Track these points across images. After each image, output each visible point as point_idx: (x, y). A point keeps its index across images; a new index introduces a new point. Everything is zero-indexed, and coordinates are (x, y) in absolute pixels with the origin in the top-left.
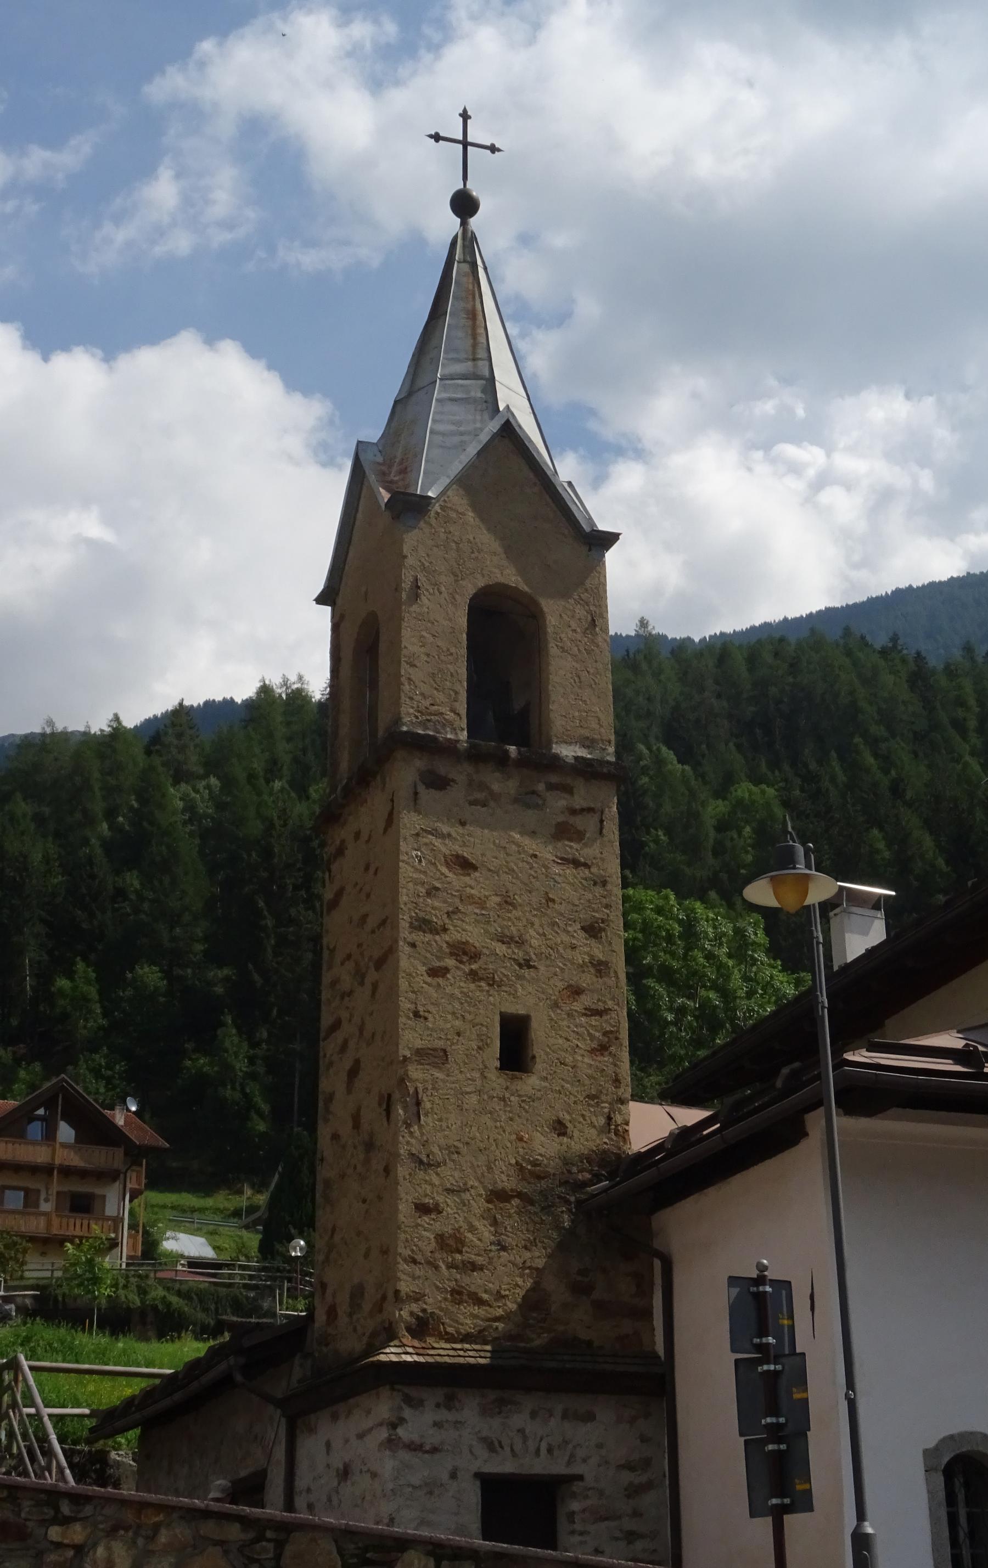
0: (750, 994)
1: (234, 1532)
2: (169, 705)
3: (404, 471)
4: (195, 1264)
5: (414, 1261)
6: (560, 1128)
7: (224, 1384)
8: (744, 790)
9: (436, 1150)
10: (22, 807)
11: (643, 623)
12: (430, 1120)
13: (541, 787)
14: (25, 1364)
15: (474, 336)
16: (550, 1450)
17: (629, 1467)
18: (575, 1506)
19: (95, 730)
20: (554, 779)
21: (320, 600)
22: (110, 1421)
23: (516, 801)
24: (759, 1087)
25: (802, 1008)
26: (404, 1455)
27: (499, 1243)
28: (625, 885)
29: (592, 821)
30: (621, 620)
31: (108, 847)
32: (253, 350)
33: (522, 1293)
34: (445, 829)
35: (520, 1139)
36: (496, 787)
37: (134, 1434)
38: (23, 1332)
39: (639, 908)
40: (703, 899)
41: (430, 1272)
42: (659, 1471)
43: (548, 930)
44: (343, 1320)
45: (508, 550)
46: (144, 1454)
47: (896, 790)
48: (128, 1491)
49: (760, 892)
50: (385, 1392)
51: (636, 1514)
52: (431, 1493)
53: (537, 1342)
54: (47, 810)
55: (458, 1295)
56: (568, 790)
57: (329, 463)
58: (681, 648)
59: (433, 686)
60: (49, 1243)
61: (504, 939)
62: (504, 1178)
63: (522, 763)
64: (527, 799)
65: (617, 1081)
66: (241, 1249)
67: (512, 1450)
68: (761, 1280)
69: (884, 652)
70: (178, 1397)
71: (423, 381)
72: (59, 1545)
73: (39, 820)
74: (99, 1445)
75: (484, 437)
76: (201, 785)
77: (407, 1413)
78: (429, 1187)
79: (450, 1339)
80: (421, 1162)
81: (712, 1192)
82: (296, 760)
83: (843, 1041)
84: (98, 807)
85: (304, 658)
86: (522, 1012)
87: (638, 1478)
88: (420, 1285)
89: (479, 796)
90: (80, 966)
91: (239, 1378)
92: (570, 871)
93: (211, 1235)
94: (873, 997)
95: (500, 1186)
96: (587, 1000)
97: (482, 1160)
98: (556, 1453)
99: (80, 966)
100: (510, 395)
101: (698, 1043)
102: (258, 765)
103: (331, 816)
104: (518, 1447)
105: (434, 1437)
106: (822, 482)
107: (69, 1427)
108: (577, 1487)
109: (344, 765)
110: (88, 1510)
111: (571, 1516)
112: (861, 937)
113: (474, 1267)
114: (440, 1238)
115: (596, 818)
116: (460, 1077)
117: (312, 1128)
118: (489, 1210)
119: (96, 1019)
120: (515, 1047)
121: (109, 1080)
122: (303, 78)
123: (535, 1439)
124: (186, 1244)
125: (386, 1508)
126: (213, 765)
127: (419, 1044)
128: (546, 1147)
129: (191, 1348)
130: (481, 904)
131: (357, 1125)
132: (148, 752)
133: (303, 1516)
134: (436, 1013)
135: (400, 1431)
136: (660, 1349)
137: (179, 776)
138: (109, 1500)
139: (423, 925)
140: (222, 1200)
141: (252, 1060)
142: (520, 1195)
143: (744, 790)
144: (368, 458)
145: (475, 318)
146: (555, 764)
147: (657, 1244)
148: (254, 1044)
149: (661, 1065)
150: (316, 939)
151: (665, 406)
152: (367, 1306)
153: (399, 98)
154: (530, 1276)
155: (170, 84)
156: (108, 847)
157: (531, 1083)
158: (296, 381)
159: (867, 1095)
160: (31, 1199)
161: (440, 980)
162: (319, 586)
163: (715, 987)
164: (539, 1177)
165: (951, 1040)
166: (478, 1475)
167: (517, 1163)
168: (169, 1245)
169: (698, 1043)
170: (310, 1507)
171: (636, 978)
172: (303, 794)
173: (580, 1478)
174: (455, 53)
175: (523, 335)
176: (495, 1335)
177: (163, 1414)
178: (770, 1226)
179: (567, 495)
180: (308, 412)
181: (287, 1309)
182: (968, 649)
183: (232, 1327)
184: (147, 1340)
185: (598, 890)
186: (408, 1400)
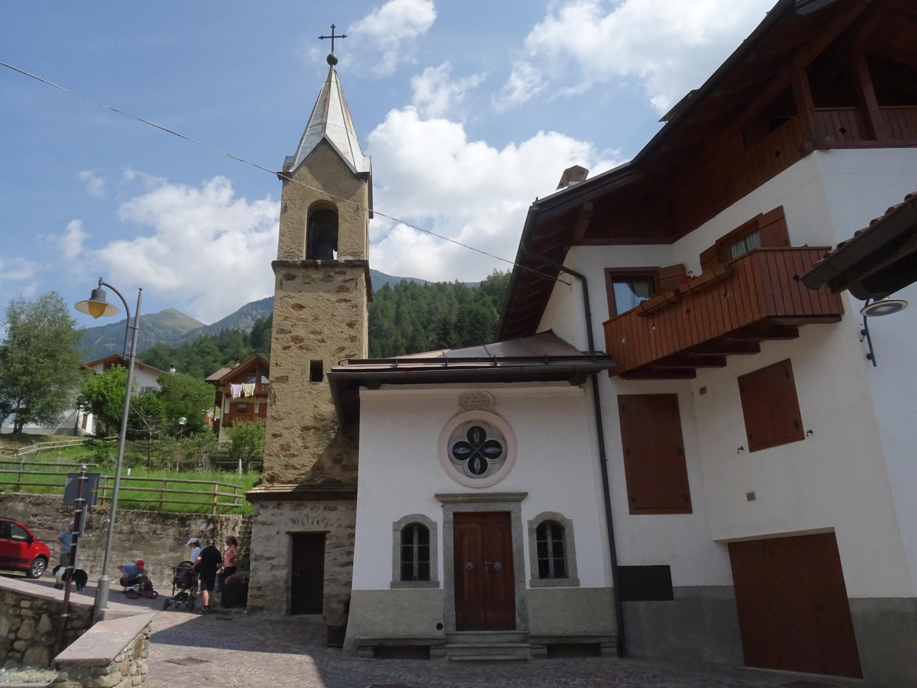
9: (281, 413)
13: (332, 274)
16: (318, 522)
20: (338, 270)
23: (322, 280)
29: (353, 283)
32: (560, 131)
34: (292, 294)
35: (316, 407)
36: (314, 276)
41: (276, 459)
43: (332, 327)
54: (496, 298)
55: (287, 466)
56: (344, 273)
61: (313, 333)
63: (324, 265)
64: (327, 279)
77: (261, 511)
78: (277, 427)
89: (307, 280)
92: (343, 304)
113: (294, 456)
114: (282, 447)
122: (577, 31)
123: (310, 519)
127: (277, 375)
130: (305, 320)
139: (282, 331)
142: (314, 428)
166: (288, 533)
173: (329, 532)
185: (354, 309)
186: (262, 506)
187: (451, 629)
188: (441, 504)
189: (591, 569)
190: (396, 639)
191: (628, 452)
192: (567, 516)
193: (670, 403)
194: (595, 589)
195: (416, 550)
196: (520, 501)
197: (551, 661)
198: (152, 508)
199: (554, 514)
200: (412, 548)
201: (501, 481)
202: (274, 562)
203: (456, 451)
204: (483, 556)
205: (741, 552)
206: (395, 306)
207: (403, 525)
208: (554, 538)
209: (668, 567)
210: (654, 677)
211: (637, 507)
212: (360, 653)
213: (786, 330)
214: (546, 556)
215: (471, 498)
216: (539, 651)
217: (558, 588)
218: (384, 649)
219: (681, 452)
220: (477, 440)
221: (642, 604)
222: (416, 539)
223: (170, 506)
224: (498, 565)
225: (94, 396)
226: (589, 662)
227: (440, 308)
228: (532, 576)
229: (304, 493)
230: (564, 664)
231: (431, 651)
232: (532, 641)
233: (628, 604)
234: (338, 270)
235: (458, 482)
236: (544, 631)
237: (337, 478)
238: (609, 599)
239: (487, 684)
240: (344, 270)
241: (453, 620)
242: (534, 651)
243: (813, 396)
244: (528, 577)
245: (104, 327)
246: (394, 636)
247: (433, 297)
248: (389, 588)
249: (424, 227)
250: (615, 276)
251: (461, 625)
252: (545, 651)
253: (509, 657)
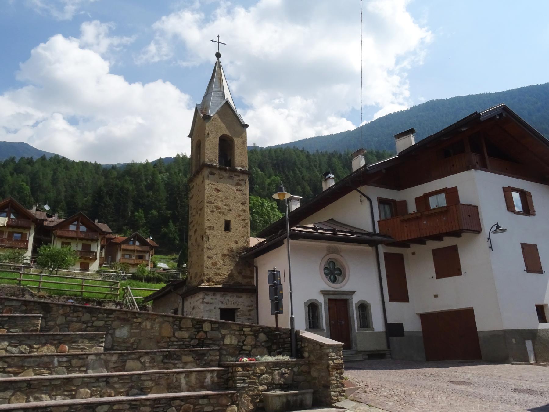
0: (274, 217)
1: (171, 319)
2: (158, 158)
3: (206, 110)
4: (164, 269)
6: (236, 242)
7: (170, 291)
8: (274, 177)
10: (128, 178)
11: (254, 144)
14: (129, 288)
15: (220, 83)
17: (249, 306)
18: (238, 314)
19: (142, 163)
20: (236, 174)
21: (189, 136)
22: (147, 299)
24: (274, 235)
25: (283, 220)
26: (205, 304)
28: (250, 195)
30: (250, 143)
31: (146, 187)
37: (152, 301)
38: (129, 282)
39: (253, 200)
40: (265, 199)
42: (255, 307)
44: (193, 279)
45: (227, 127)
46: (154, 305)
47: (303, 178)
48: (150, 312)
49: (276, 196)
50: (202, 293)
51: (250, 315)
54: (133, 179)
55: (216, 274)
56: (239, 176)
57: (190, 109)
58: (262, 149)
59: (212, 155)
60: (134, 265)
61: (225, 205)
64: (230, 178)
65: (247, 233)
66: (174, 266)
68: (274, 271)
69: (301, 151)
70: (161, 294)
71: (210, 92)
72: (136, 322)
73: (131, 181)
74: (145, 304)
75: (222, 104)
76: (165, 174)
77: (206, 297)
78: (210, 253)
79: (214, 282)
81: (265, 254)
82: (184, 170)
83: (291, 225)
84: (143, 178)
85: (185, 148)
86: (229, 219)
87: (251, 308)
88: (209, 272)
90: (140, 210)
91: (172, 290)
92: (239, 192)
93: (167, 263)
94: (298, 217)
96: (242, 217)
97: (221, 248)
99: (140, 210)
100: (227, 96)
101: (264, 226)
102: (176, 170)
103: (191, 180)
105: (211, 301)
106: (288, 116)
107: (138, 300)
108: (239, 310)
109: (194, 170)
110: (142, 315)
111: (237, 316)
112: (295, 206)
113: (219, 269)
114: (213, 264)
117: (187, 242)
119: (143, 221)
120: (228, 226)
121: (146, 233)
123: (230, 301)
124: (162, 265)
125: (202, 314)
126: (167, 170)
127: (209, 226)
128: (234, 246)
129: (163, 285)
130: (221, 198)
131: (196, 241)
132: (154, 167)
133: (185, 316)
134: (212, 220)
135: (204, 300)
136: (255, 284)
137: (160, 172)
138: (146, 314)
139: (209, 202)
140: (170, 257)
141: (176, 229)
142: (228, 255)
143: (274, 177)
144: (199, 107)
145: (220, 79)
146: (236, 171)
147: (255, 264)
148: (176, 226)
149: (257, 231)
150: (188, 205)
151: (258, 99)
152: (198, 276)
153: (205, 31)
155: (157, 25)
156: (146, 187)
157: (231, 233)
158: (183, 90)
159: (296, 236)
160: (130, 257)
162: (189, 133)
163: (267, 216)
164: (232, 252)
165: (312, 226)
168: (159, 265)
169: (264, 226)
170: (187, 315)
171: (252, 213)
172: (186, 176)
174: (216, 23)
175: (230, 82)
177: (157, 298)
178: (278, 260)
179: (239, 116)
180: (186, 97)
181: (182, 277)
182: (317, 151)
183: (171, 281)
184: (154, 283)
186: (206, 294)
189: (378, 325)
191: (388, 277)
192: (369, 302)
196: (352, 295)
198: (76, 295)
201: (346, 286)
205: (425, 318)
206: (52, 172)
209: (402, 323)
213: (457, 234)
215: (335, 293)
219: (405, 278)
224: (343, 322)
227: (86, 178)
233: (391, 338)
236: (363, 349)
237: (240, 282)
238: (384, 336)
243: (466, 259)
244: (356, 327)
247: (81, 171)
249: (73, 121)
250: (382, 202)
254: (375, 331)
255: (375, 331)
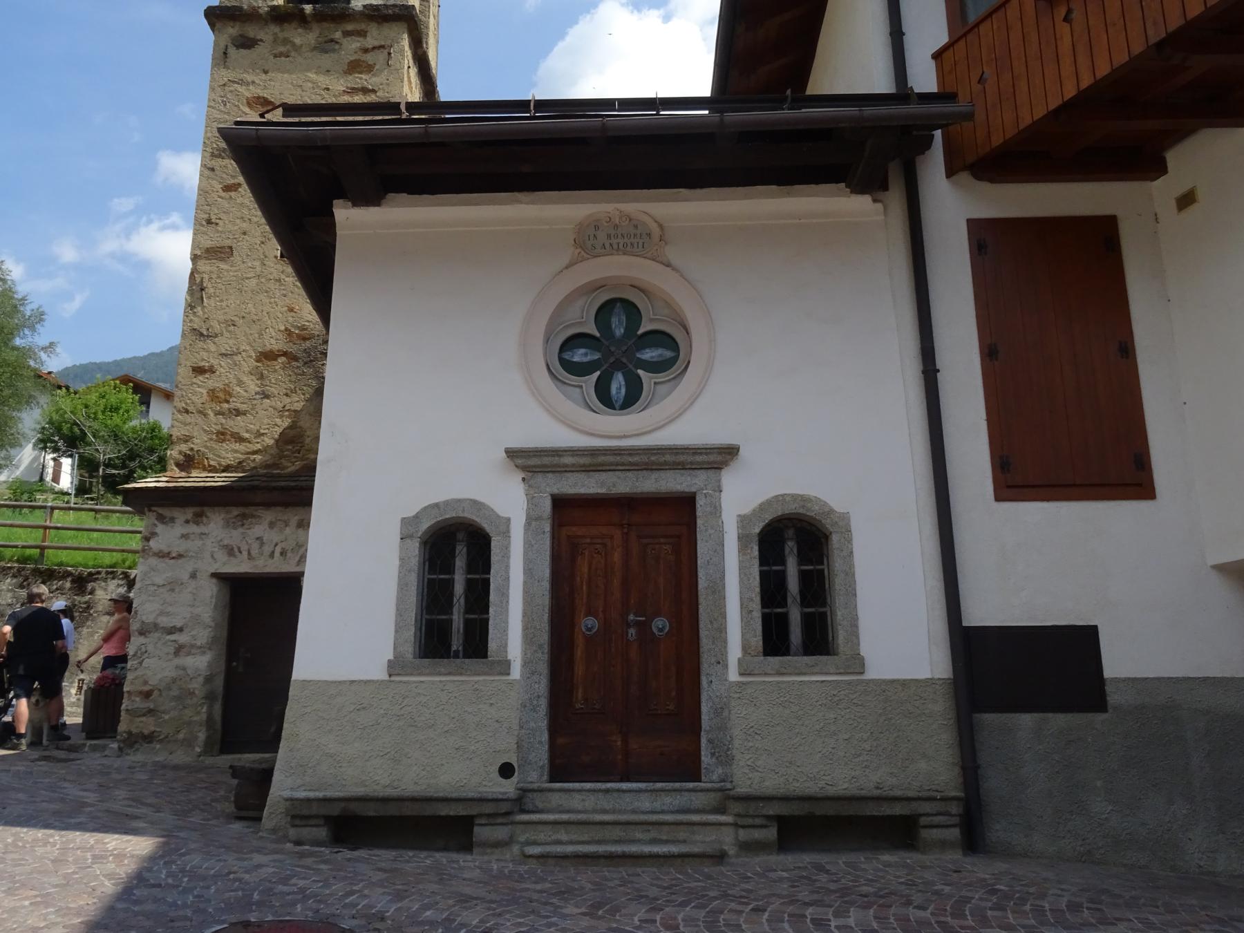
5: (187, 412)
12: (212, 302)
13: (338, 35)
16: (283, 553)
20: (350, 27)
26: (153, 561)
27: (263, 393)
29: (381, 56)
33: (279, 430)
34: (249, 78)
35: (291, 310)
36: (298, 41)
41: (200, 419)
52: (173, 590)
53: (292, 469)
55: (222, 435)
56: (362, 34)
62: (273, 341)
64: (326, 46)
67: (249, 554)
77: (160, 528)
80: (202, 335)
89: (282, 49)
95: (268, 347)
98: (289, 555)
104: (254, 552)
105: (179, 546)
113: (238, 413)
114: (213, 395)
115: (386, 52)
116: (242, 266)
118: (257, 367)
135: (152, 543)
142: (285, 354)
154: (288, 417)
161: (233, 194)
166: (215, 575)
167: (286, 329)
176: (252, 465)
186: (161, 519)
187: (535, 774)
188: (521, 475)
189: (895, 630)
190: (385, 800)
193: (1101, 236)
194: (904, 684)
195: (459, 588)
196: (718, 467)
197: (789, 859)
198: (24, 560)
199: (804, 499)
200: (451, 583)
201: (675, 418)
202: (182, 638)
203: (566, 356)
204: (623, 605)
207: (425, 525)
208: (802, 559)
210: (1074, 907)
211: (1014, 481)
212: (292, 832)
214: (783, 603)
216: (757, 834)
217: (808, 677)
218: (356, 824)
220: (619, 331)
221: (1026, 720)
222: (460, 563)
223: (64, 556)
224: (660, 624)
225: (65, 428)
226: (888, 865)
228: (745, 648)
229: (253, 489)
230: (821, 868)
231: (476, 829)
232: (737, 807)
233: (989, 719)
234: (350, 27)
235: (566, 421)
236: (771, 784)
238: (940, 708)
239: (585, 922)
240: (363, 26)
241: (541, 755)
242: (743, 834)
244: (734, 652)
245: (145, 357)
246: (390, 792)
248: (384, 676)
251: (563, 768)
252: (771, 833)
253: (674, 849)
254: (872, 673)
255: (872, 673)
